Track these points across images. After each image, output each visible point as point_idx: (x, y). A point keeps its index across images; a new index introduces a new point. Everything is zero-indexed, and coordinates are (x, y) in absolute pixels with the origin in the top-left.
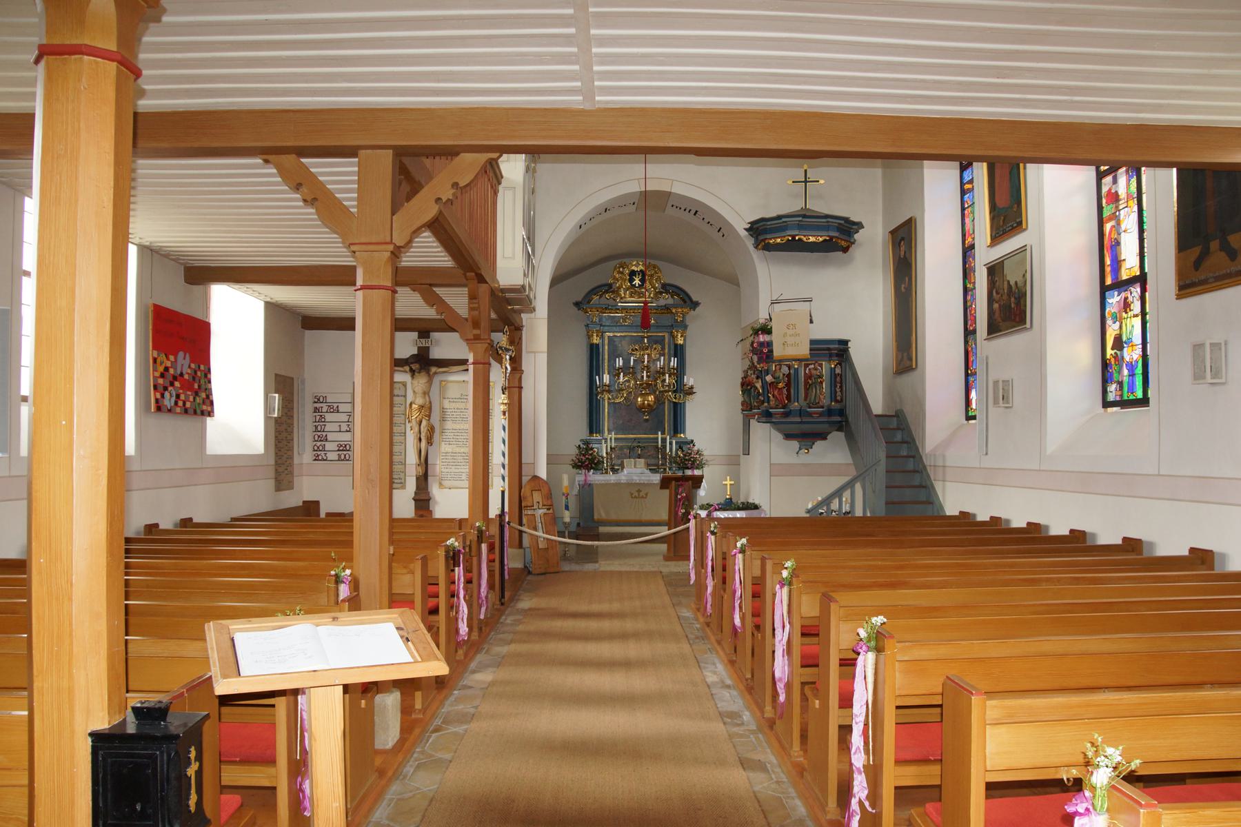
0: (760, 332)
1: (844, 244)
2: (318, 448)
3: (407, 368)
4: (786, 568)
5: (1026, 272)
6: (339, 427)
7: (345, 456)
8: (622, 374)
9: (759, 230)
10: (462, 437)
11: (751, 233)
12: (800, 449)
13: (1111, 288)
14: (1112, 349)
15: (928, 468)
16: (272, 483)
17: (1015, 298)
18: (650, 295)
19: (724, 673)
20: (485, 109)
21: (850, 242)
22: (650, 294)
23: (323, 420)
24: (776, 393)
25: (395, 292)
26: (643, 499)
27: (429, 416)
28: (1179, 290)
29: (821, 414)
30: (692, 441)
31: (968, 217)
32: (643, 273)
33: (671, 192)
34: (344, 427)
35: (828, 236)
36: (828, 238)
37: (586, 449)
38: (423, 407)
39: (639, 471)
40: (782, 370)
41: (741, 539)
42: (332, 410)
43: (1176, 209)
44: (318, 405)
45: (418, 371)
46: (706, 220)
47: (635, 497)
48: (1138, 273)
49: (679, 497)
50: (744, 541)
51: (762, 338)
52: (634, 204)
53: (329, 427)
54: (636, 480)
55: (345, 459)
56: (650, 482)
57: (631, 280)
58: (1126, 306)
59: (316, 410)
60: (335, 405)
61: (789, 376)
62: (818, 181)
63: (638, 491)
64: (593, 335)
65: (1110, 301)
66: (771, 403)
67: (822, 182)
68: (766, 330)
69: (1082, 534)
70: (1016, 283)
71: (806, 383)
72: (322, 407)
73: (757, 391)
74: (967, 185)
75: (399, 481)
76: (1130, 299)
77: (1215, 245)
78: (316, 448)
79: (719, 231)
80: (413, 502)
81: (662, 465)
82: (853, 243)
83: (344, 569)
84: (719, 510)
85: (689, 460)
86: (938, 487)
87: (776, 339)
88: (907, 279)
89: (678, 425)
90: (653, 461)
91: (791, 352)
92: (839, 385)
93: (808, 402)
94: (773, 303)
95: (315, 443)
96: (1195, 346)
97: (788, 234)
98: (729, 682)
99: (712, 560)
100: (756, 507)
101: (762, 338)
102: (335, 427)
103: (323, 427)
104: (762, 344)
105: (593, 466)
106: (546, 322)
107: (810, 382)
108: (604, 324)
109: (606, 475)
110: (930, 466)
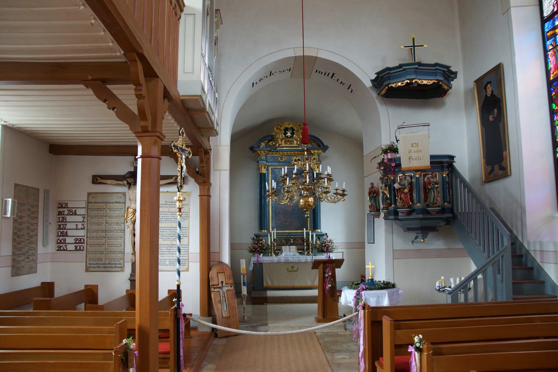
0: (389, 151)
2: (61, 241)
3: (125, 182)
6: (76, 226)
7: (80, 247)
8: (288, 179)
10: (166, 233)
12: (416, 238)
18: (297, 143)
22: (297, 142)
23: (65, 220)
24: (403, 196)
25: (160, 159)
26: (295, 273)
29: (438, 212)
33: (317, 57)
34: (80, 226)
35: (437, 80)
36: (436, 82)
37: (258, 240)
39: (292, 254)
42: (71, 213)
44: (61, 210)
46: (340, 81)
49: (326, 275)
53: (69, 226)
54: (291, 260)
55: (80, 250)
57: (285, 133)
59: (60, 213)
60: (74, 210)
62: (423, 46)
63: (292, 267)
66: (398, 204)
67: (425, 46)
68: (393, 149)
72: (64, 211)
73: (385, 196)
75: (120, 266)
78: (59, 241)
80: (129, 282)
81: (307, 249)
85: (325, 246)
87: (402, 154)
88: (496, 110)
89: (316, 225)
91: (415, 164)
95: (58, 238)
97: (407, 78)
102: (73, 226)
103: (64, 226)
104: (390, 160)
105: (263, 251)
107: (430, 187)
108: (268, 161)
109: (271, 257)
110: (535, 251)
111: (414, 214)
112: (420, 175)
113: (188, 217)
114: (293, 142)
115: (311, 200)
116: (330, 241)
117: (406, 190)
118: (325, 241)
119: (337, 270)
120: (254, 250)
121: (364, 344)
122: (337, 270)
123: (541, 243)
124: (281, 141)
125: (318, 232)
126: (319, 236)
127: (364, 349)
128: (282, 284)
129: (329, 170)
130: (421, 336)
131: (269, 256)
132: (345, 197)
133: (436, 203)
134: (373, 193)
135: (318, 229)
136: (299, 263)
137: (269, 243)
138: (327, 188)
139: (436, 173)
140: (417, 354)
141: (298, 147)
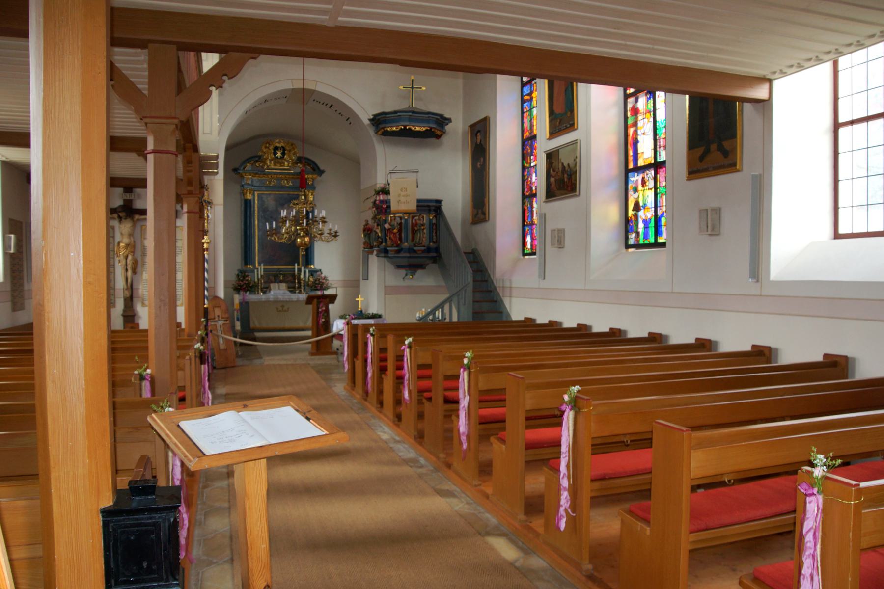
0: (380, 193)
1: (439, 133)
4: (467, 357)
5: (576, 157)
9: (378, 121)
11: (373, 122)
12: (406, 275)
13: (634, 170)
14: (633, 210)
15: (498, 289)
16: (8, 305)
17: (568, 175)
19: (391, 432)
20: (252, 19)
21: (442, 131)
24: (392, 236)
27: (133, 252)
28: (689, 174)
29: (423, 252)
30: (320, 270)
31: (527, 118)
32: (284, 149)
36: (429, 129)
38: (128, 245)
39: (282, 292)
40: (396, 220)
41: (408, 338)
43: (687, 122)
45: (124, 217)
46: (338, 112)
47: (280, 311)
48: (653, 162)
49: (320, 310)
50: (410, 339)
51: (381, 197)
52: (286, 97)
56: (291, 300)
57: (275, 153)
58: (644, 183)
61: (400, 224)
63: (282, 307)
64: (246, 193)
65: (632, 179)
67: (424, 88)
68: (385, 191)
69: (619, 331)
70: (569, 165)
71: (413, 229)
73: (377, 235)
74: (526, 97)
76: (646, 178)
77: (714, 147)
79: (347, 120)
81: (298, 288)
82: (444, 133)
83: (145, 370)
84: (355, 318)
85: (319, 284)
86: (506, 301)
87: (393, 198)
88: (482, 159)
89: (308, 259)
90: (291, 285)
91: (403, 207)
92: (434, 231)
93: (414, 243)
94: (391, 173)
96: (700, 210)
98: (397, 438)
99: (371, 354)
100: (380, 316)
101: (381, 197)
104: (382, 202)
105: (249, 288)
106: (222, 182)
107: (416, 229)
110: (500, 287)
111: (402, 252)
112: (409, 217)
113: (181, 252)
114: (284, 163)
115: (307, 239)
116: (325, 278)
117: (395, 230)
118: (319, 278)
119: (330, 306)
120: (239, 287)
121: (348, 351)
122: (330, 306)
123: (503, 280)
124: (270, 162)
125: (311, 268)
126: (313, 273)
127: (348, 355)
128: (271, 325)
129: (323, 214)
130: (374, 328)
131: (255, 294)
132: (337, 238)
133: (422, 243)
134: (368, 230)
135: (311, 265)
136: (290, 302)
137: (256, 280)
138: (321, 230)
139: (423, 215)
140: (372, 338)
141: (290, 170)
